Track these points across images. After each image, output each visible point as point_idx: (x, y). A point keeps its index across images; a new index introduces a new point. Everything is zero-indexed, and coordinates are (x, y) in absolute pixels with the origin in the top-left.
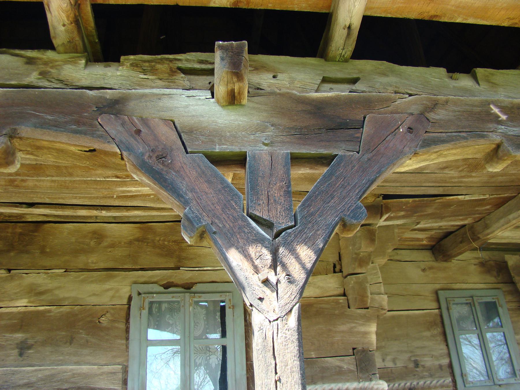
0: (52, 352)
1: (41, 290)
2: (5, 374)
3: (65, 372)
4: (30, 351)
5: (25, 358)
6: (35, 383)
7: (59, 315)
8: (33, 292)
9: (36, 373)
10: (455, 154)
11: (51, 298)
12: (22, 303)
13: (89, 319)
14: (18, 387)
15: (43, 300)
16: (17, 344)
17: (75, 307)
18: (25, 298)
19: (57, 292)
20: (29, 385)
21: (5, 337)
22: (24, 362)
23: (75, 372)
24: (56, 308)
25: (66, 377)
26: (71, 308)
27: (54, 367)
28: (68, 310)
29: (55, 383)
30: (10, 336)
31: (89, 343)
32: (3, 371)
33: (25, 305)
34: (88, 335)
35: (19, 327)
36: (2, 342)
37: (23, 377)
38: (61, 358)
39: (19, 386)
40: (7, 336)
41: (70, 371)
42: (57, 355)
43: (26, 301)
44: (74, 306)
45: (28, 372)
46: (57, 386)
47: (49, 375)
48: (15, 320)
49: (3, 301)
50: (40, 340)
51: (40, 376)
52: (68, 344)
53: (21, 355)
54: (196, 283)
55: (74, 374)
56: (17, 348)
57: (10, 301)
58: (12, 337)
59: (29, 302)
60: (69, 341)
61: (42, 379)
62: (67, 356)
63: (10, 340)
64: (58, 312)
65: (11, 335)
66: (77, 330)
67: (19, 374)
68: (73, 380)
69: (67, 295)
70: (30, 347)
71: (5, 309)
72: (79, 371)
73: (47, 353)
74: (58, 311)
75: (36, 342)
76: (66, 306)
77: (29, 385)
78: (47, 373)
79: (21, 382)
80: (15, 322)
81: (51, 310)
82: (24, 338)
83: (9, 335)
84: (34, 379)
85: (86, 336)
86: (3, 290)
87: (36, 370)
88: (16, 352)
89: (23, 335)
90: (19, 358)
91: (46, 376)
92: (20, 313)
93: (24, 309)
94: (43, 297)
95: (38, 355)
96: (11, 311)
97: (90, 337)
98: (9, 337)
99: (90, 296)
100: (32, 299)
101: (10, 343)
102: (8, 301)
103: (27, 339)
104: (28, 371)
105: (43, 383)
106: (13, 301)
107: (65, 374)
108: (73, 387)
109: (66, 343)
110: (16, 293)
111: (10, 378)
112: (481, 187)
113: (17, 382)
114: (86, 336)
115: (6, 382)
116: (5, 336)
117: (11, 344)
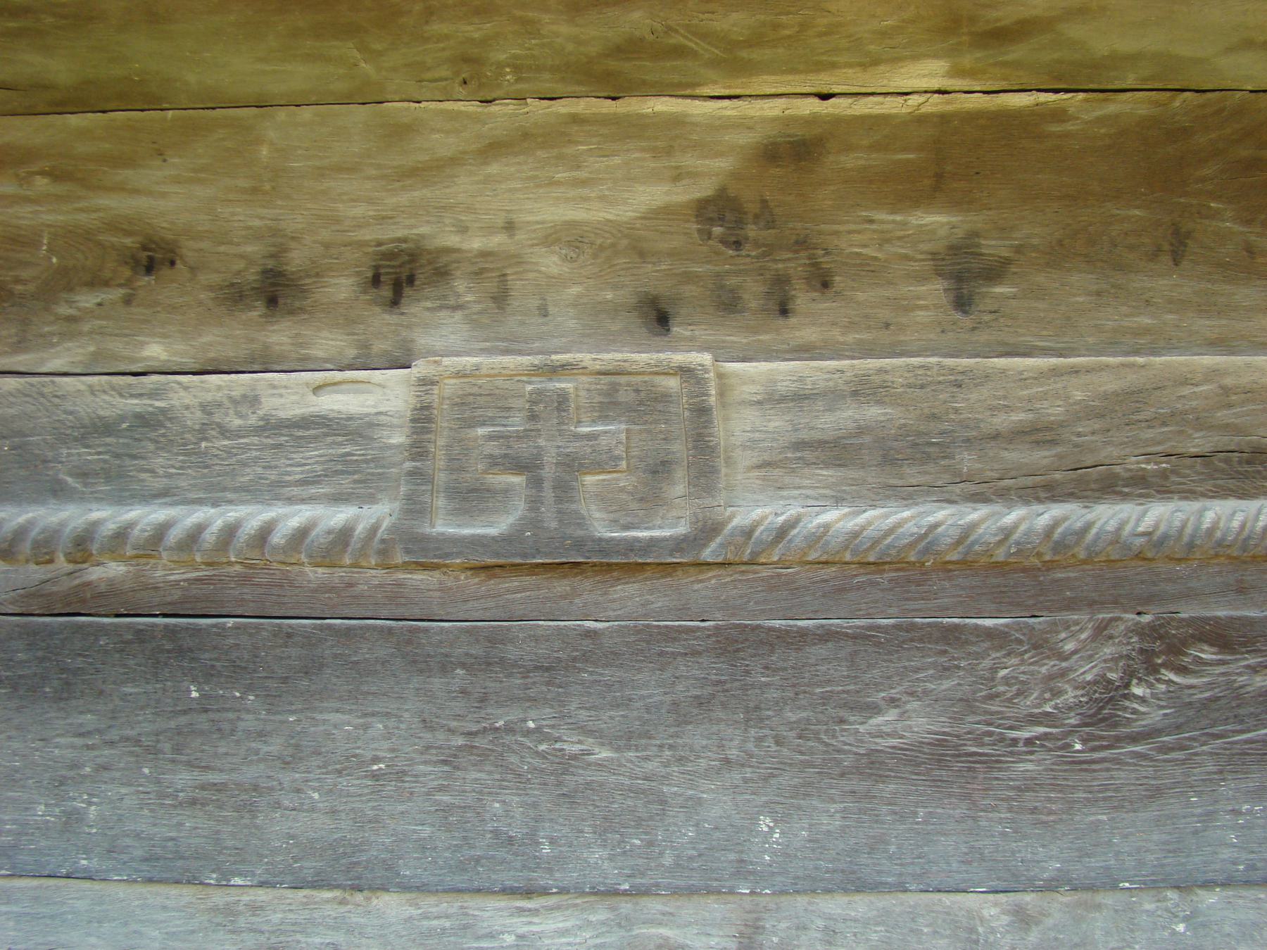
0: (1099, 294)
1: (998, 20)
2: (922, 387)
3: (1185, 382)
4: (998, 290)
5: (987, 318)
6: (1061, 425)
7: (1102, 131)
8: (965, 30)
9: (1059, 385)
10: (876, 743)
11: (1056, 56)
12: (924, 76)
13: (1244, 152)
14: (993, 443)
15: (1017, 65)
16: (934, 255)
17: (1172, 99)
18: (936, 56)
19: (1075, 31)
20: (1040, 436)
21: (874, 227)
22: (983, 337)
23: (1228, 381)
24: (1086, 100)
25: (1194, 403)
26: (1157, 104)
27: (1131, 359)
28: (1143, 111)
29: (1149, 427)
30: (894, 222)
31: (1260, 260)
32: (911, 369)
33: (936, 84)
34: (1248, 222)
35: (927, 182)
36: (865, 246)
37: (1005, 397)
38: (1146, 321)
39: (996, 436)
40: (882, 222)
41: (1207, 380)
42: (1124, 309)
43: (940, 66)
44: (1168, 94)
45: (1022, 379)
46: (1159, 443)
47: (1116, 394)
48: (905, 150)
49: (834, 66)
50: (1035, 241)
51: (1078, 395)
52: (1166, 259)
53: (962, 303)
54: (759, 403)
55: (1226, 391)
56: (940, 274)
57: (864, 66)
58: (905, 224)
59: (957, 72)
60: (1166, 247)
61: (1088, 412)
62: (1171, 312)
63: (900, 238)
64: (1100, 121)
65: (898, 218)
66: (1195, 202)
67: (981, 384)
68: (1222, 415)
69: (1125, 45)
70: (995, 272)
71: (850, 101)
72: (1245, 380)
73: (1080, 299)
74: (1098, 113)
75: (1019, 250)
76: (1129, 94)
77: (1040, 436)
78: (1110, 384)
79: (1001, 421)
80: (908, 160)
81: (1064, 111)
82: (960, 233)
83: (891, 217)
84: (1055, 411)
85: (1237, 228)
86: (825, 21)
87: (1055, 372)
88: (935, 290)
89: (954, 219)
90: (958, 316)
91: (1105, 397)
92: (921, 120)
93: (937, 104)
94: (1017, 52)
95: (1041, 305)
96: (877, 110)
97: (1259, 230)
98: (890, 227)
99: (1230, 50)
100: (967, 61)
101: (904, 251)
102: (858, 69)
103: (974, 234)
104: (1021, 373)
105: (1097, 426)
106: (882, 68)
107: (1186, 391)
108: (1232, 448)
109: (1155, 255)
110: (884, 34)
111: (945, 402)
112: (863, 90)
113: (982, 420)
114: (1241, 229)
115: (934, 417)
116: (871, 221)
117: (906, 258)
